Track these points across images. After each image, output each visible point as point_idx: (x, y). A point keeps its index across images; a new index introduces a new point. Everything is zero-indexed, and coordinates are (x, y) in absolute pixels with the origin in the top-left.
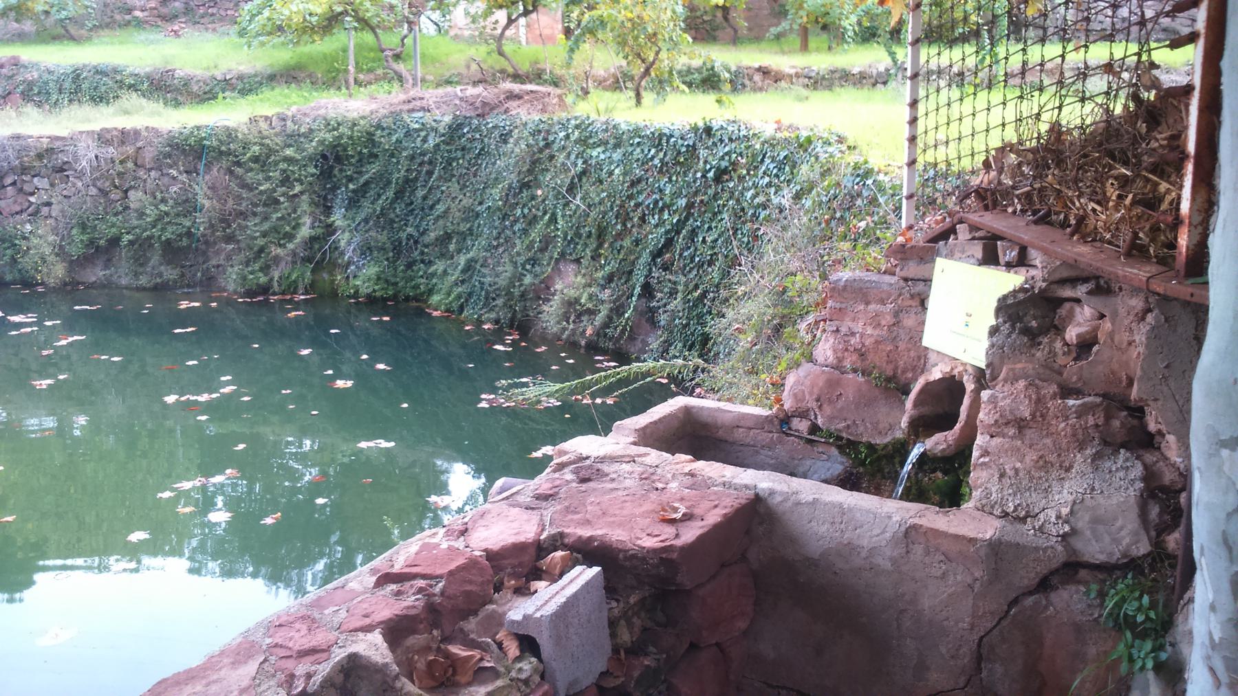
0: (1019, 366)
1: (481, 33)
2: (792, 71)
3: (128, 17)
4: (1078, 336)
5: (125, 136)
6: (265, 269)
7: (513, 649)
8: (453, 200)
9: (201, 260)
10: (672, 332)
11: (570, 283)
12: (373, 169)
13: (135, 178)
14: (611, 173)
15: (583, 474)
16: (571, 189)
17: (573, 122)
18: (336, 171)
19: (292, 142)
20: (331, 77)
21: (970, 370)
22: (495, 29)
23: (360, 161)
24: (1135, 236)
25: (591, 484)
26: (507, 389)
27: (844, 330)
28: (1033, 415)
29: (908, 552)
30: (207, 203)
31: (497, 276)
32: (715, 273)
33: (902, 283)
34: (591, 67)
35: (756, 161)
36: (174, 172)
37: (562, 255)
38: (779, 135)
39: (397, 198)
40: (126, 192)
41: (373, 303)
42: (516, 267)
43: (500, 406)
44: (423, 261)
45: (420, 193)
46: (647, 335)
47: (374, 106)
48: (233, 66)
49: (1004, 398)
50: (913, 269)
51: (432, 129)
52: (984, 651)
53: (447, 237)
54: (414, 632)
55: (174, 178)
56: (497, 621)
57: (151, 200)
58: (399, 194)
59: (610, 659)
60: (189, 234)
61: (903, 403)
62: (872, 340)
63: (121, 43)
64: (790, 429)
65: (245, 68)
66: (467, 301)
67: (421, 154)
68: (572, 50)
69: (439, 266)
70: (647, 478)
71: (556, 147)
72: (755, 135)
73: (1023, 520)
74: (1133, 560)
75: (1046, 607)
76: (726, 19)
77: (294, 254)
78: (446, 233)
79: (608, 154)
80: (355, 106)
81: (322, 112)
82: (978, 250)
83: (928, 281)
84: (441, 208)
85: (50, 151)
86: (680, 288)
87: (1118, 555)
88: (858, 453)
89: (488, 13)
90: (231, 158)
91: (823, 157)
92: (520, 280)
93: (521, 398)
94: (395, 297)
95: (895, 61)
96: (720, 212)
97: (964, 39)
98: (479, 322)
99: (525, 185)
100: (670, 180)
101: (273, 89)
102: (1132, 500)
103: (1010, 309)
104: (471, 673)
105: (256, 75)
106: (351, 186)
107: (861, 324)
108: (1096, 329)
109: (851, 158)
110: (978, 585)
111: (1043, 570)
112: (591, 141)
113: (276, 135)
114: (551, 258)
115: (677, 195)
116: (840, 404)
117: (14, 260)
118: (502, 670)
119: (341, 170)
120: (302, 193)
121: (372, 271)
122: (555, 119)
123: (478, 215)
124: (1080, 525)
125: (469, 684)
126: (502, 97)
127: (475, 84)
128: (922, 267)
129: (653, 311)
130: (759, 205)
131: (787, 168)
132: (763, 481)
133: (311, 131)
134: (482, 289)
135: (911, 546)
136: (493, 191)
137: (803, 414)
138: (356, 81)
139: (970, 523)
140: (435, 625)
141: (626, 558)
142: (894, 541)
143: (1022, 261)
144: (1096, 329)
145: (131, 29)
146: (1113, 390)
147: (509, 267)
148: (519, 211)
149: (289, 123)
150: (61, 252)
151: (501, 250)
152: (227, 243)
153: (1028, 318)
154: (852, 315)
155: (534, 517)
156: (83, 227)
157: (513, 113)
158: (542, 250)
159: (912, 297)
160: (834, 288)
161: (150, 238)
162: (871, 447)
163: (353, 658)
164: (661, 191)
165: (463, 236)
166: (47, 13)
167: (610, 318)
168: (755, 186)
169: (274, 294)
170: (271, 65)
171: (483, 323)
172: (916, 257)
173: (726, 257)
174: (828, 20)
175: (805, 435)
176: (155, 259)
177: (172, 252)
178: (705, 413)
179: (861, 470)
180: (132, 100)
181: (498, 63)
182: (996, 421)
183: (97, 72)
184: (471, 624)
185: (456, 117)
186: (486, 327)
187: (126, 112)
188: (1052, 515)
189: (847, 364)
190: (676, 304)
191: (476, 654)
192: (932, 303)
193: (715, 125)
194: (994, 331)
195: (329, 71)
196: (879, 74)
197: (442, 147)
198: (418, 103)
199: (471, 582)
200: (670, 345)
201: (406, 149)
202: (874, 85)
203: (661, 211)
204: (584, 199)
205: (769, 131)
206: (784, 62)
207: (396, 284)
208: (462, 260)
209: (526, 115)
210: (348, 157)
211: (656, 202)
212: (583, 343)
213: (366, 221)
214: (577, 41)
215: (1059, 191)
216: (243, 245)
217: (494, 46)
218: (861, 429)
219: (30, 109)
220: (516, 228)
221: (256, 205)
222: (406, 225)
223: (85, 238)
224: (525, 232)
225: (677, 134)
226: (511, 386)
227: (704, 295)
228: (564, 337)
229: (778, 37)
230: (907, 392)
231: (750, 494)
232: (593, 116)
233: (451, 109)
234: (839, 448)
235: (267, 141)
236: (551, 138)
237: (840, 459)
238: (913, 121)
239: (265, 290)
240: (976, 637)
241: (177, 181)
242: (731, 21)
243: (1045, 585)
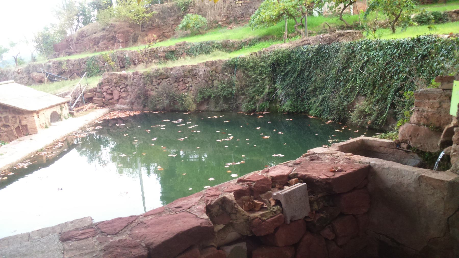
3: (217, 25)
5: (213, 63)
6: (254, 104)
7: (273, 203)
8: (318, 76)
9: (235, 101)
11: (362, 104)
12: (289, 67)
13: (215, 76)
14: (378, 60)
15: (313, 158)
16: (362, 68)
17: (363, 42)
18: (277, 69)
19: (263, 60)
20: (279, 37)
22: (339, 11)
23: (285, 64)
25: (314, 161)
27: (421, 110)
30: (236, 83)
33: (442, 91)
34: (376, 20)
36: (227, 74)
37: (359, 93)
39: (298, 76)
40: (213, 81)
41: (289, 114)
42: (341, 99)
44: (307, 99)
45: (306, 74)
47: (291, 45)
48: (248, 37)
50: (446, 86)
51: (311, 51)
53: (316, 89)
54: (245, 195)
55: (227, 76)
56: (270, 195)
57: (220, 83)
58: (299, 75)
59: (309, 213)
60: (231, 93)
62: (431, 113)
63: (215, 33)
65: (251, 37)
66: (322, 112)
67: (306, 60)
69: (313, 100)
71: (356, 52)
72: (439, 40)
77: (263, 98)
78: (315, 88)
79: (377, 53)
80: (283, 46)
81: (273, 49)
83: (451, 90)
84: (313, 79)
85: (192, 70)
86: (406, 104)
89: (337, 5)
90: (244, 67)
94: (297, 112)
99: (345, 68)
101: (170, 47)
104: (259, 208)
105: (255, 39)
106: (282, 74)
110: (445, 198)
112: (370, 49)
113: (258, 58)
114: (355, 95)
116: (418, 138)
117: (182, 104)
118: (269, 208)
119: (279, 69)
120: (266, 77)
121: (289, 103)
125: (258, 211)
133: (269, 56)
135: (421, 183)
137: (405, 142)
138: (288, 37)
140: (252, 194)
145: (218, 28)
147: (338, 99)
149: (262, 54)
150: (195, 101)
151: (335, 93)
152: (243, 95)
154: (423, 104)
155: (291, 169)
156: (201, 93)
157: (341, 41)
158: (351, 92)
160: (416, 95)
161: (220, 95)
162: (430, 153)
163: (224, 198)
165: (321, 89)
166: (194, 26)
167: (377, 117)
169: (257, 112)
170: (260, 35)
176: (221, 102)
177: (226, 99)
179: (426, 162)
180: (217, 51)
181: (340, 23)
183: (207, 44)
184: (263, 196)
187: (215, 56)
191: (262, 203)
195: (279, 35)
197: (314, 57)
198: (306, 42)
199: (264, 184)
201: (301, 59)
203: (399, 73)
204: (367, 71)
207: (297, 107)
208: (321, 97)
209: (345, 42)
210: (281, 64)
212: (367, 127)
213: (287, 85)
216: (247, 96)
218: (426, 147)
219: (189, 58)
221: (251, 83)
222: (301, 86)
223: (201, 96)
224: (345, 85)
225: (405, 42)
231: (367, 165)
233: (318, 42)
234: (418, 154)
235: (255, 61)
237: (418, 158)
239: (254, 111)
241: (227, 76)
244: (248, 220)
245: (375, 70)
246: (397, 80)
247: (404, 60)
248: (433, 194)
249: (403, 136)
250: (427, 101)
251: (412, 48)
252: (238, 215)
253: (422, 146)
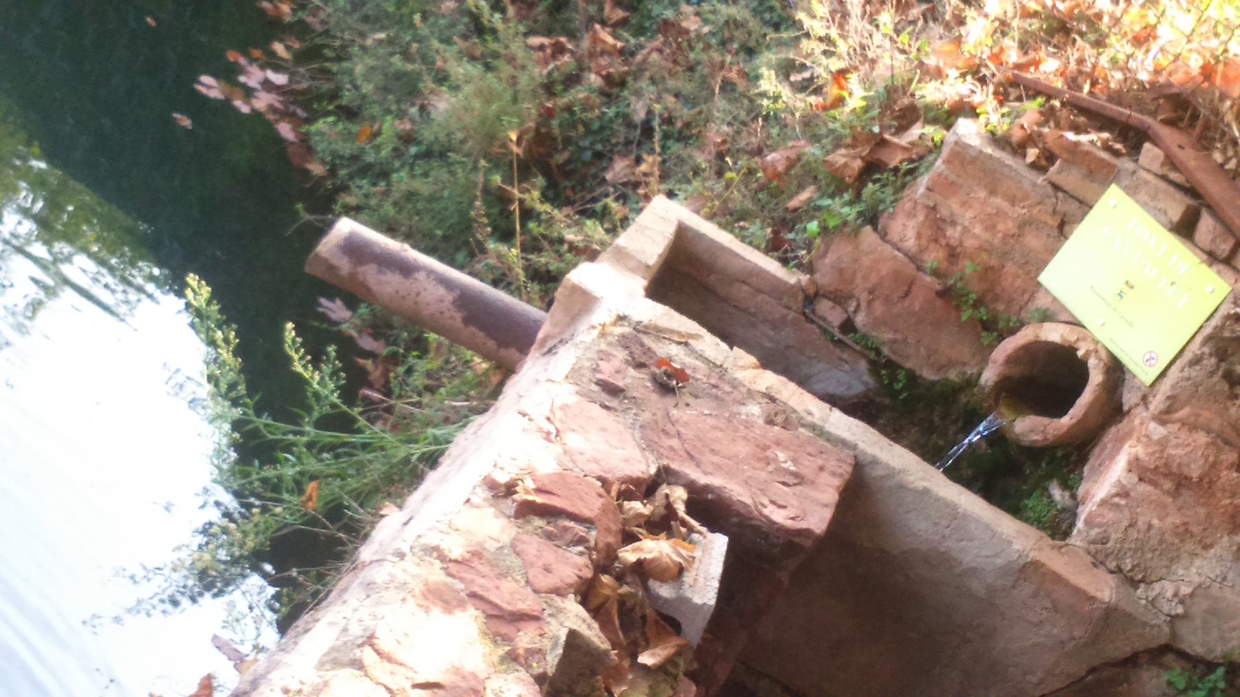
21: (1103, 355)
28: (1201, 479)
29: (1014, 587)
33: (1049, 190)
49: (1177, 446)
50: (1071, 179)
64: (813, 311)
82: (1176, 207)
83: (1086, 206)
88: (894, 379)
107: (969, 214)
111: (1139, 646)
124: (1194, 610)
135: (1021, 581)
142: (1005, 570)
159: (1054, 212)
162: (913, 378)
175: (838, 335)
179: (887, 401)
182: (1157, 468)
192: (1081, 235)
248: (1041, 623)
250: (982, 194)
253: (895, 341)
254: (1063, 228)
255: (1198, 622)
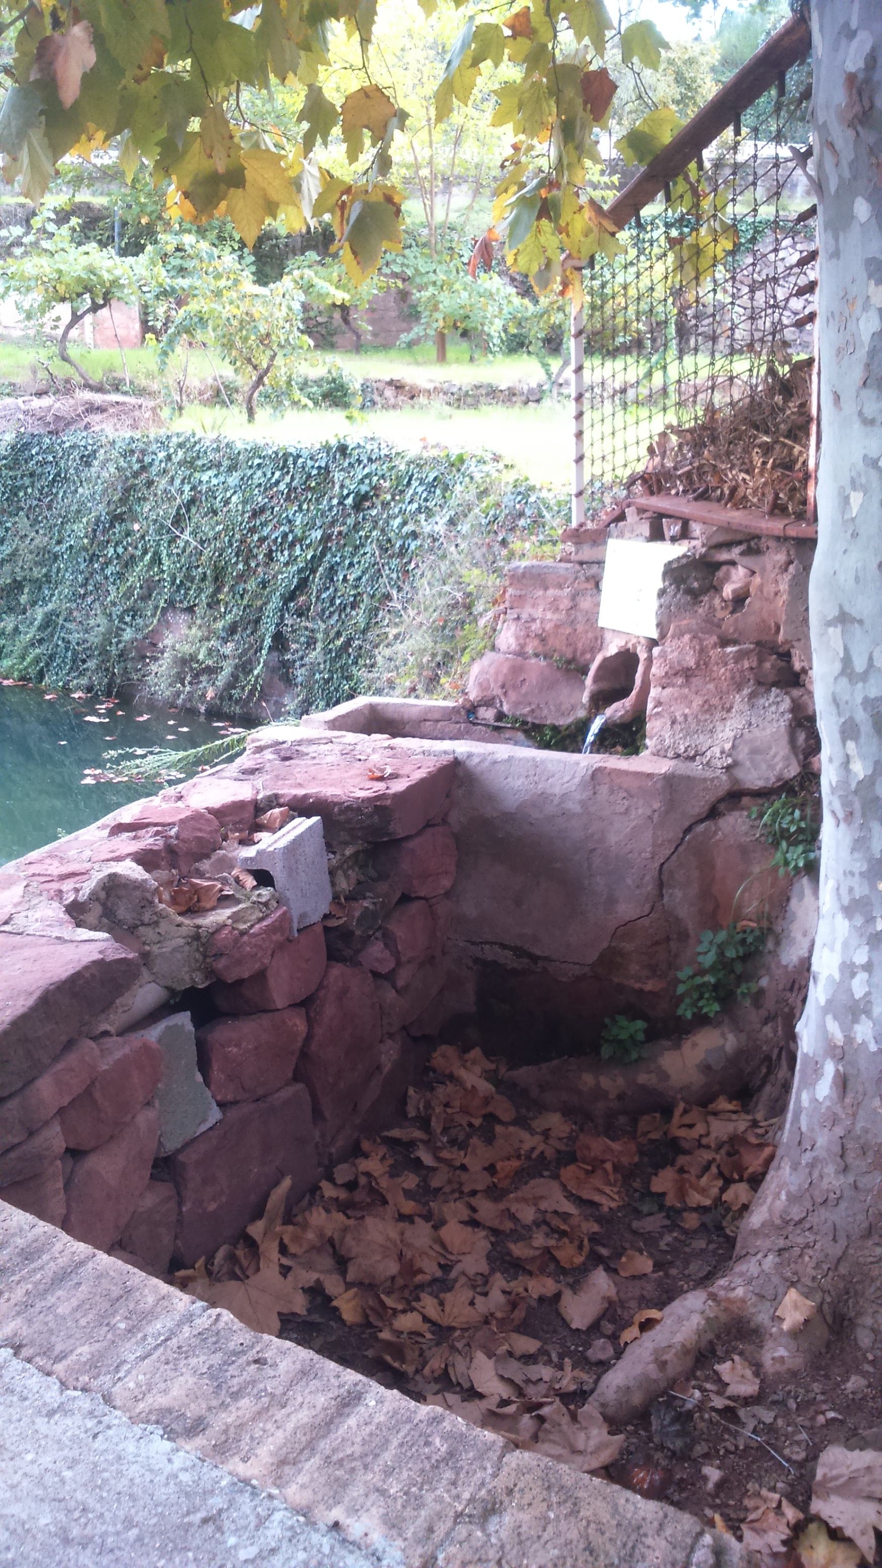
0: (685, 622)
1: (38, 332)
2: (430, 386)
4: (734, 591)
7: (250, 882)
10: (311, 688)
11: (182, 637)
14: (227, 502)
15: (283, 754)
17: (175, 440)
21: (643, 641)
22: (56, 327)
24: (777, 497)
26: (117, 761)
27: (524, 616)
28: (698, 664)
31: (87, 631)
32: (359, 616)
33: (577, 567)
35: (402, 484)
37: (171, 604)
38: (425, 455)
43: (109, 783)
46: (281, 695)
50: (587, 553)
52: (665, 878)
61: (583, 682)
68: (165, 353)
70: (348, 754)
71: (154, 470)
72: (398, 454)
73: (693, 759)
74: (787, 782)
75: (715, 833)
76: (346, 321)
78: (15, 581)
79: (222, 479)
82: (645, 529)
83: (600, 563)
86: (320, 636)
87: (773, 779)
89: (46, 306)
91: (478, 477)
92: (118, 635)
93: (135, 771)
95: (549, 375)
96: (363, 545)
97: (625, 350)
98: (67, 690)
99: (117, 518)
100: (300, 509)
102: (783, 729)
103: (676, 573)
108: (748, 585)
109: (509, 477)
111: (711, 797)
112: (200, 463)
114: (156, 607)
115: (310, 526)
116: (524, 689)
122: (152, 437)
123: (56, 557)
125: (213, 909)
126: (80, 410)
127: (40, 394)
128: (595, 550)
129: (286, 665)
130: (408, 536)
131: (438, 492)
132: (461, 748)
134: (67, 649)
136: (75, 527)
137: (488, 702)
139: (647, 762)
141: (341, 812)
142: (583, 785)
143: (685, 534)
144: (748, 585)
146: (764, 638)
147: (102, 620)
148: (111, 551)
153: (692, 581)
158: (145, 598)
159: (587, 579)
163: (113, 877)
164: (290, 521)
165: (38, 585)
167: (235, 677)
168: (402, 512)
171: (70, 691)
172: (590, 537)
173: (373, 596)
174: (469, 325)
175: (492, 722)
178: (391, 709)
185: (20, 435)
186: (76, 696)
188: (717, 751)
189: (530, 650)
190: (315, 655)
192: (605, 585)
193: (351, 443)
194: (662, 593)
196: (531, 391)
200: (310, 704)
202: (526, 403)
203: (292, 545)
204: (194, 533)
205: (413, 450)
206: (419, 373)
208: (39, 613)
209: (111, 431)
211: (285, 536)
212: (203, 709)
214: (171, 342)
215: (715, 466)
217: (55, 350)
218: (545, 712)
220: (108, 572)
224: (120, 576)
225: (305, 453)
226: (123, 757)
227: (348, 643)
228: (180, 702)
229: (410, 345)
230: (585, 671)
232: (199, 434)
233: (12, 426)
234: (526, 732)
236: (147, 459)
238: (579, 435)
240: (657, 865)
242: (353, 324)
243: (713, 813)
244: (197, 937)
245: (219, 533)
246: (287, 564)
247: (305, 507)
248: (627, 811)
249: (483, 686)
250: (541, 593)
251: (325, 471)
252: (163, 927)
253: (533, 711)
254: (596, 583)
255: (748, 764)
